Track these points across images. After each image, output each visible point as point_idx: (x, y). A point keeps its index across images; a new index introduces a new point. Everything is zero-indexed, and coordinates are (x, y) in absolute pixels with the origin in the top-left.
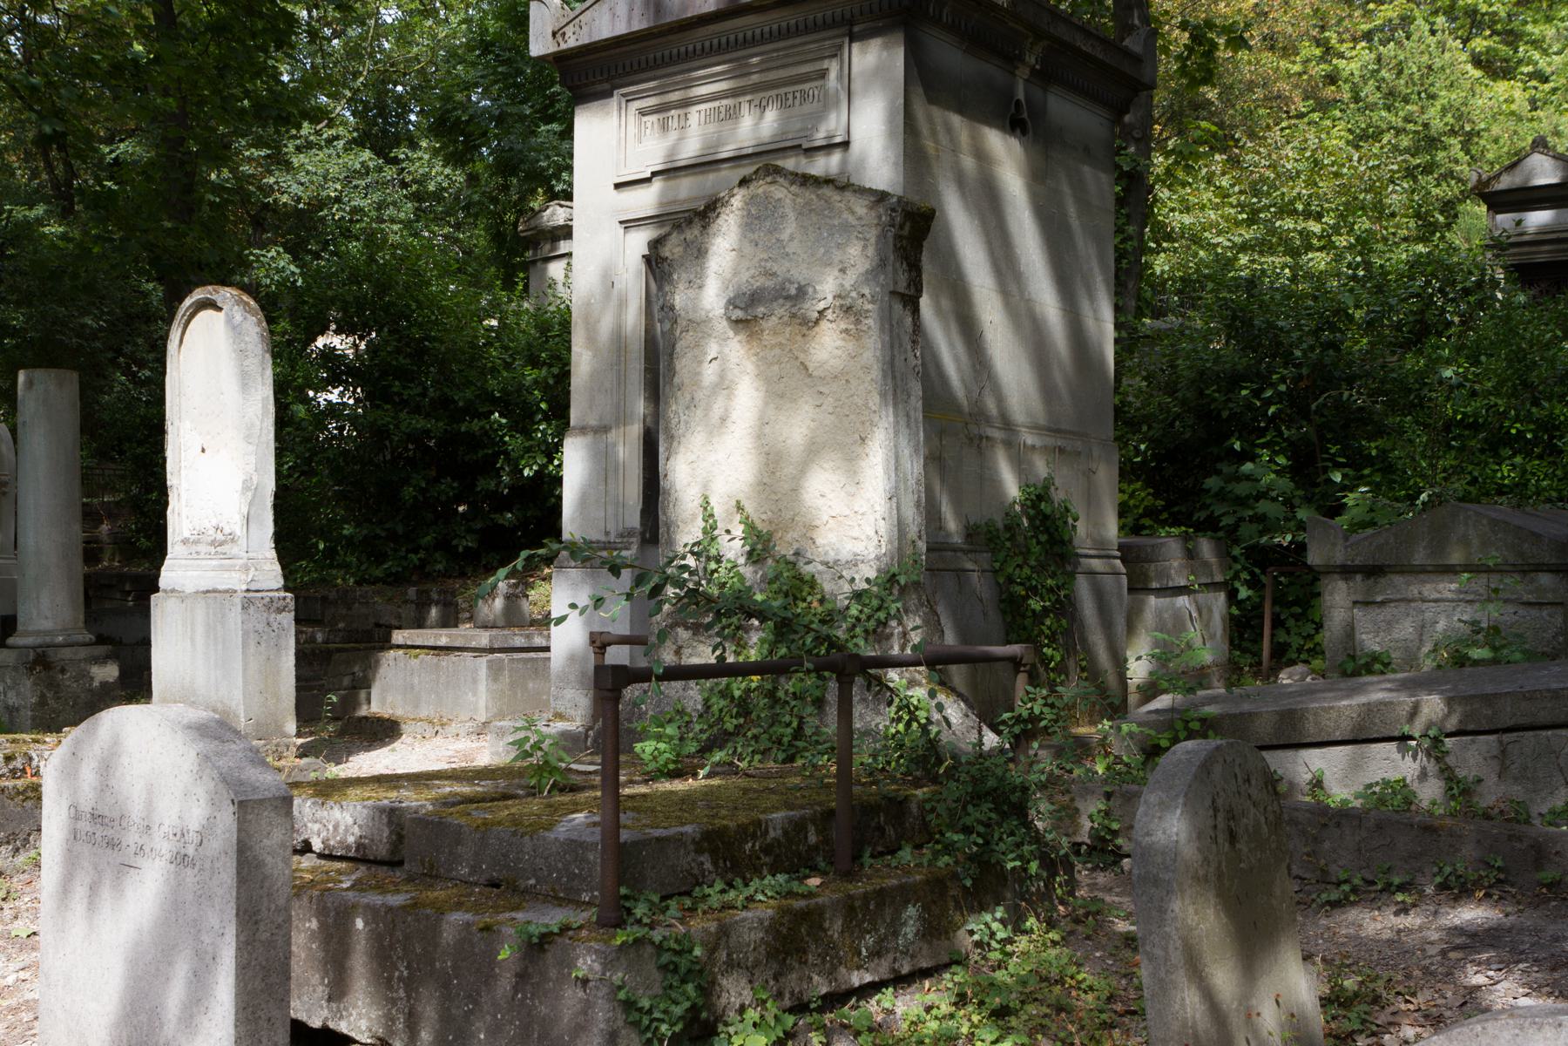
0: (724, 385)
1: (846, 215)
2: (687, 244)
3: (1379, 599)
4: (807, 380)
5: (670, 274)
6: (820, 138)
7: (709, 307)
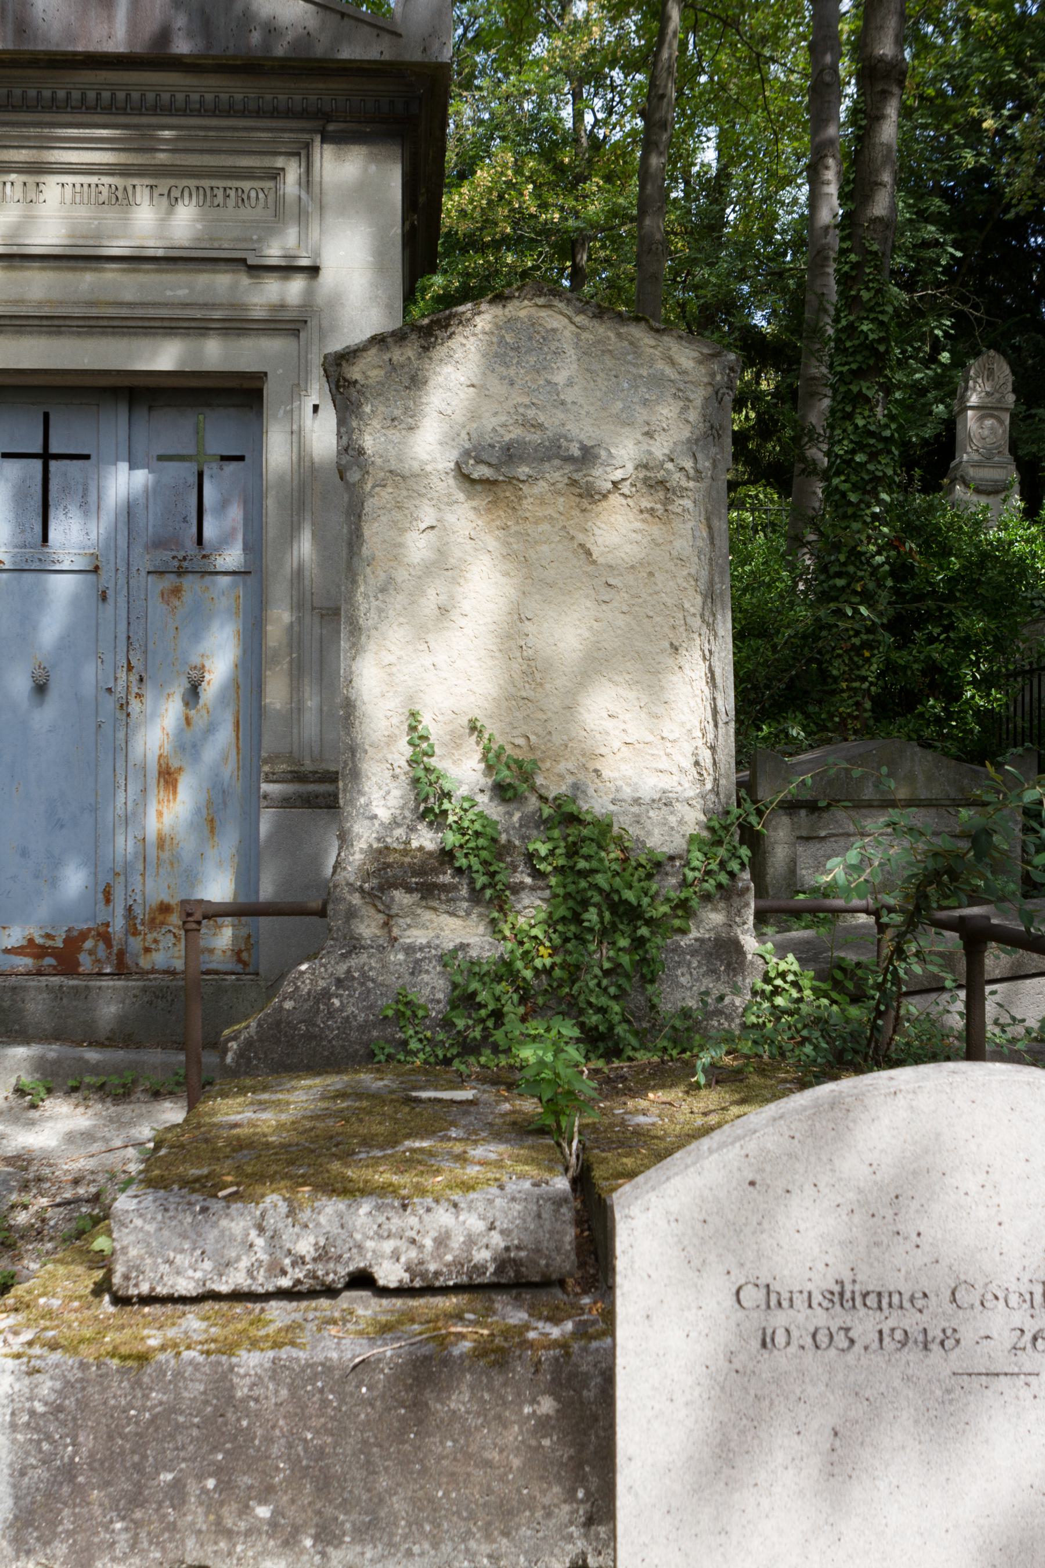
0: (443, 565)
1: (660, 365)
2: (393, 367)
3: (823, 834)
4: (590, 568)
5: (360, 405)
6: (274, 252)
7: (425, 457)
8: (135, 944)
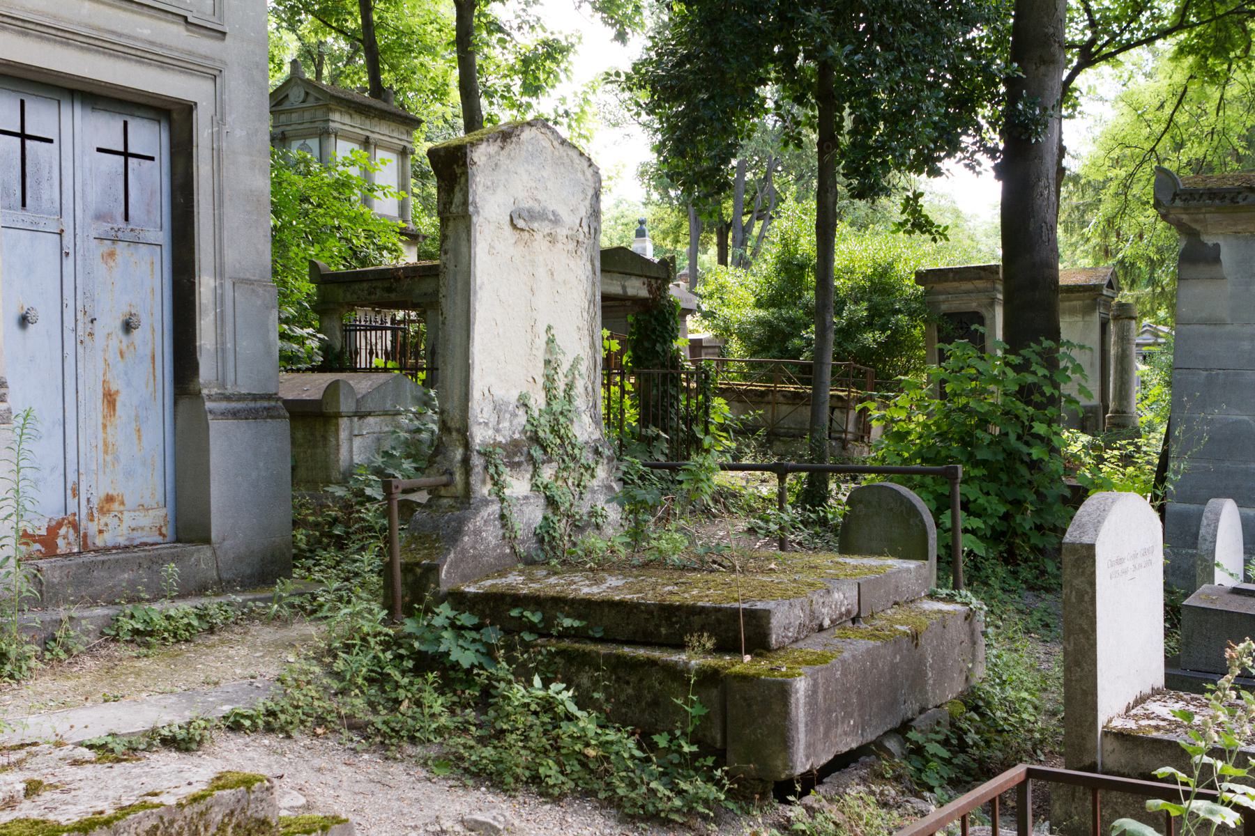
8: (93, 528)
